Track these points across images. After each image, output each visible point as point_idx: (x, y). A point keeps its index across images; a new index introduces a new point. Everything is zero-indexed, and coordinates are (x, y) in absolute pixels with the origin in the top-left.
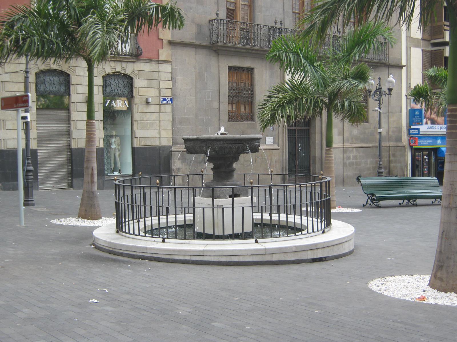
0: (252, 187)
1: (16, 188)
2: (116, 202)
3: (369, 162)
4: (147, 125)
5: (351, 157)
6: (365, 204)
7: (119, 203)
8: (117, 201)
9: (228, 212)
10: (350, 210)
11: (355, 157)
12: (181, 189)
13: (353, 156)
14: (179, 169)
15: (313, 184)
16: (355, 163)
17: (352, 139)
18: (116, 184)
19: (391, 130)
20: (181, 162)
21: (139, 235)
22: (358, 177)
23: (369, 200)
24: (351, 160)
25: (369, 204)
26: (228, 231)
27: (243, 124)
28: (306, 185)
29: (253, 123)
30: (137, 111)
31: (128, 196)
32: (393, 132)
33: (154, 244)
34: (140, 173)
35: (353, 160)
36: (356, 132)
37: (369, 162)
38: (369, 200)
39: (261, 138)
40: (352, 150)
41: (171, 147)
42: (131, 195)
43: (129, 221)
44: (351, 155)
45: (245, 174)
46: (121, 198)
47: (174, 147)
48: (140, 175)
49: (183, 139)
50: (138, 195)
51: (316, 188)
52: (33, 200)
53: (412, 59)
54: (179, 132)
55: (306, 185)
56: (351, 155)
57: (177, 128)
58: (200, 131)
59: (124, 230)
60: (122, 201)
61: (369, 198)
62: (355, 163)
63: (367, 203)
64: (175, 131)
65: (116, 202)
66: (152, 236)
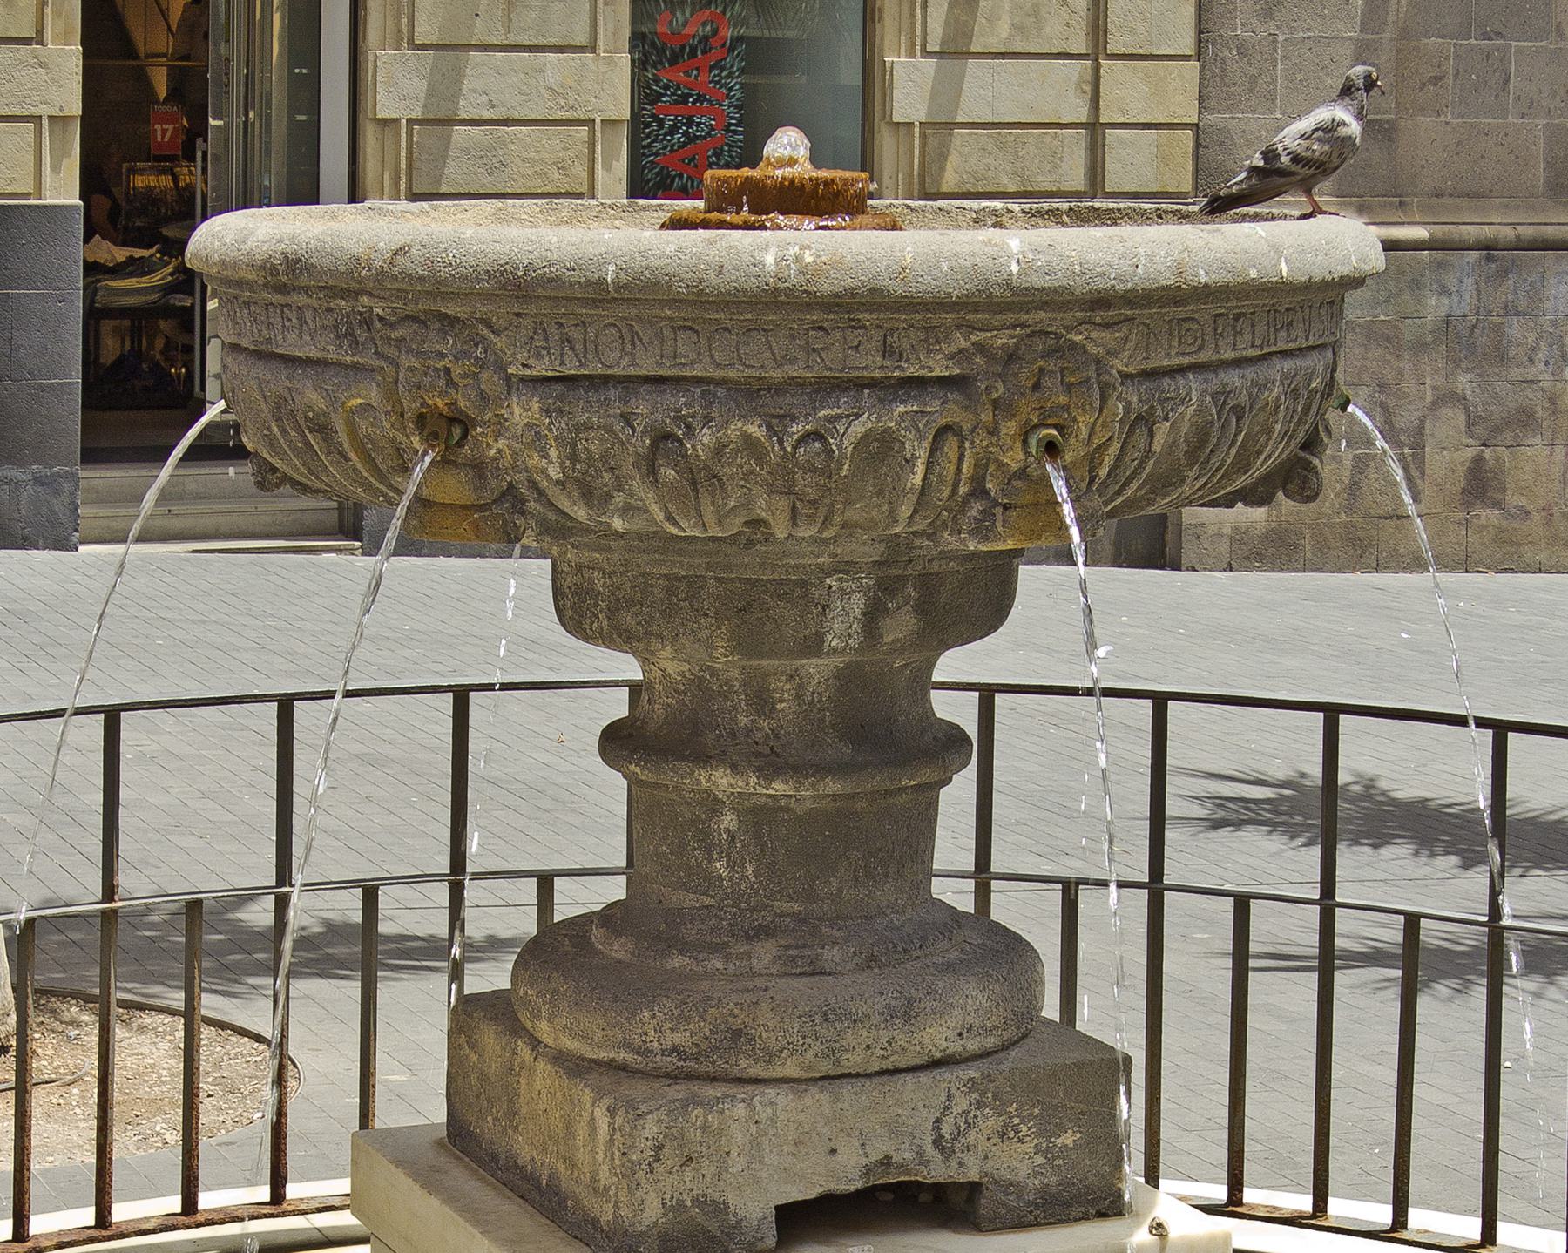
54: (1253, 80)
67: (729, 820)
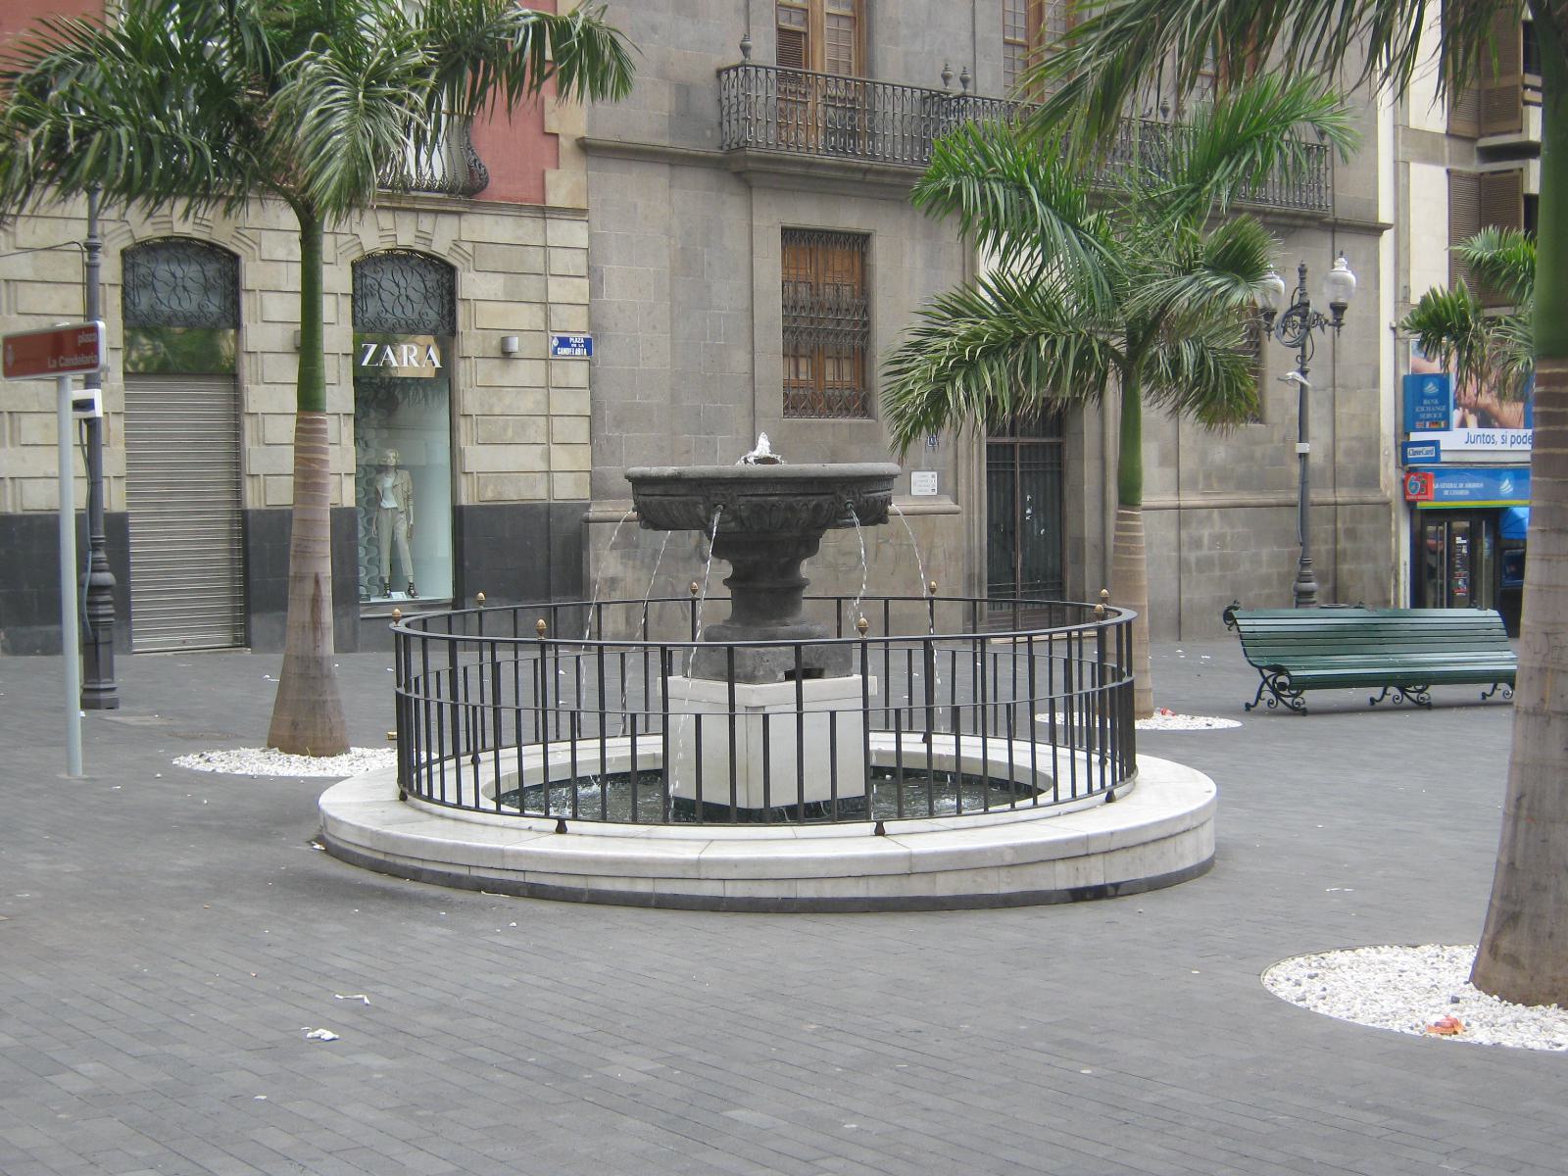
0: (864, 644)
1: (54, 647)
2: (398, 694)
3: (1264, 558)
4: (505, 429)
5: (1206, 541)
6: (1252, 703)
7: (408, 699)
8: (402, 690)
9: (783, 729)
10: (1200, 723)
11: (1219, 539)
12: (623, 649)
13: (1210, 535)
14: (613, 582)
15: (1075, 634)
16: (1217, 562)
17: (1207, 477)
18: (397, 634)
19: (1342, 446)
20: (622, 558)
21: (477, 808)
22: (1230, 608)
23: (1266, 687)
24: (1205, 552)
25: (1266, 702)
26: (784, 796)
27: (834, 425)
28: (1051, 637)
29: (869, 424)
30: (468, 382)
31: (438, 673)
32: (1349, 453)
33: (530, 840)
34: (481, 594)
35: (1210, 549)
36: (1223, 455)
37: (1264, 558)
38: (1266, 687)
39: (895, 476)
40: (1209, 517)
41: (588, 506)
42: (450, 671)
44: (1206, 534)
45: (839, 600)
46: (417, 680)
47: (597, 504)
48: (480, 602)
49: (628, 477)
50: (473, 672)
51: (1084, 648)
53: (1412, 203)
54: (613, 453)
55: (1051, 637)
56: (1206, 534)
57: (608, 439)
58: (687, 452)
59: (425, 792)
60: (417, 692)
61: (1266, 680)
62: (1217, 562)
63: (1259, 697)
64: (601, 450)
65: (398, 694)
66: (522, 811)
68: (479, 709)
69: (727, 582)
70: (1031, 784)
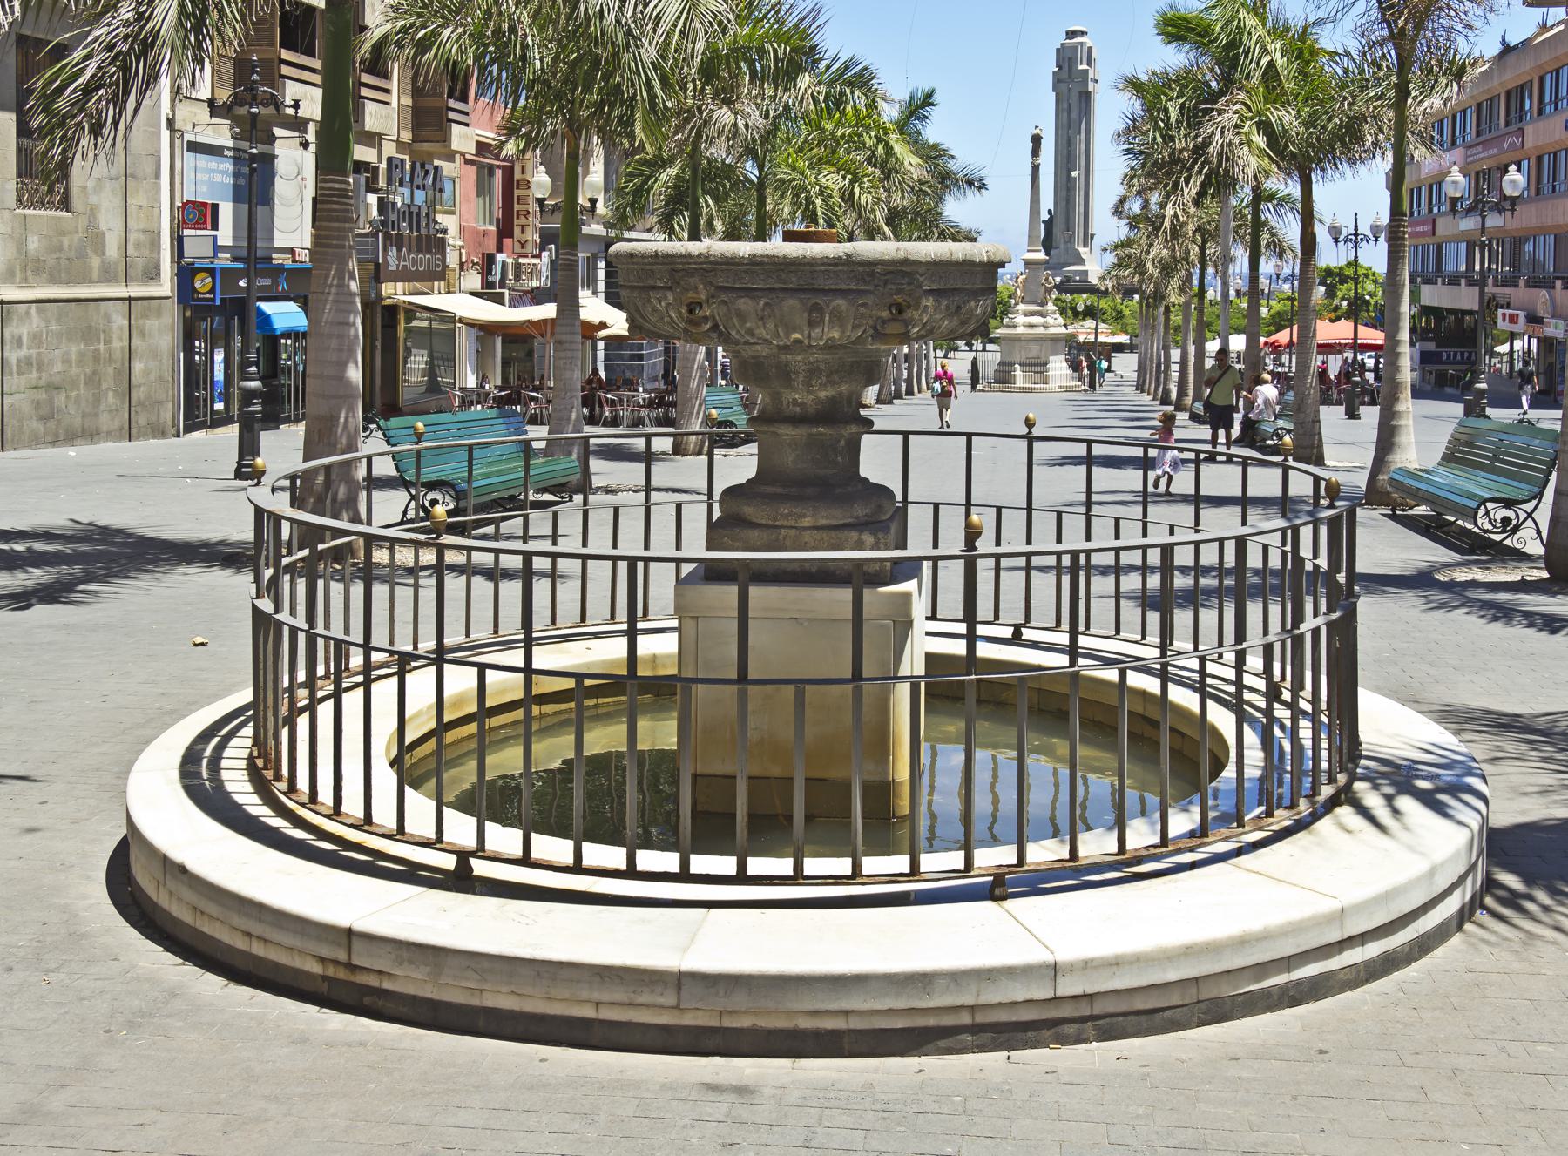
0: (935, 560)
1: (708, 549)
2: (257, 612)
5: (25, 340)
7: (279, 624)
8: (266, 605)
11: (36, 338)
17: (24, 269)
19: (132, 237)
28: (1029, 561)
32: (138, 245)
36: (36, 245)
40: (28, 313)
43: (311, 683)
44: (24, 332)
51: (940, 573)
52: (466, 114)
55: (1029, 561)
56: (24, 332)
60: (293, 613)
65: (257, 612)
67: (842, 443)
68: (302, 637)
69: (1352, 414)
70: (534, 836)
